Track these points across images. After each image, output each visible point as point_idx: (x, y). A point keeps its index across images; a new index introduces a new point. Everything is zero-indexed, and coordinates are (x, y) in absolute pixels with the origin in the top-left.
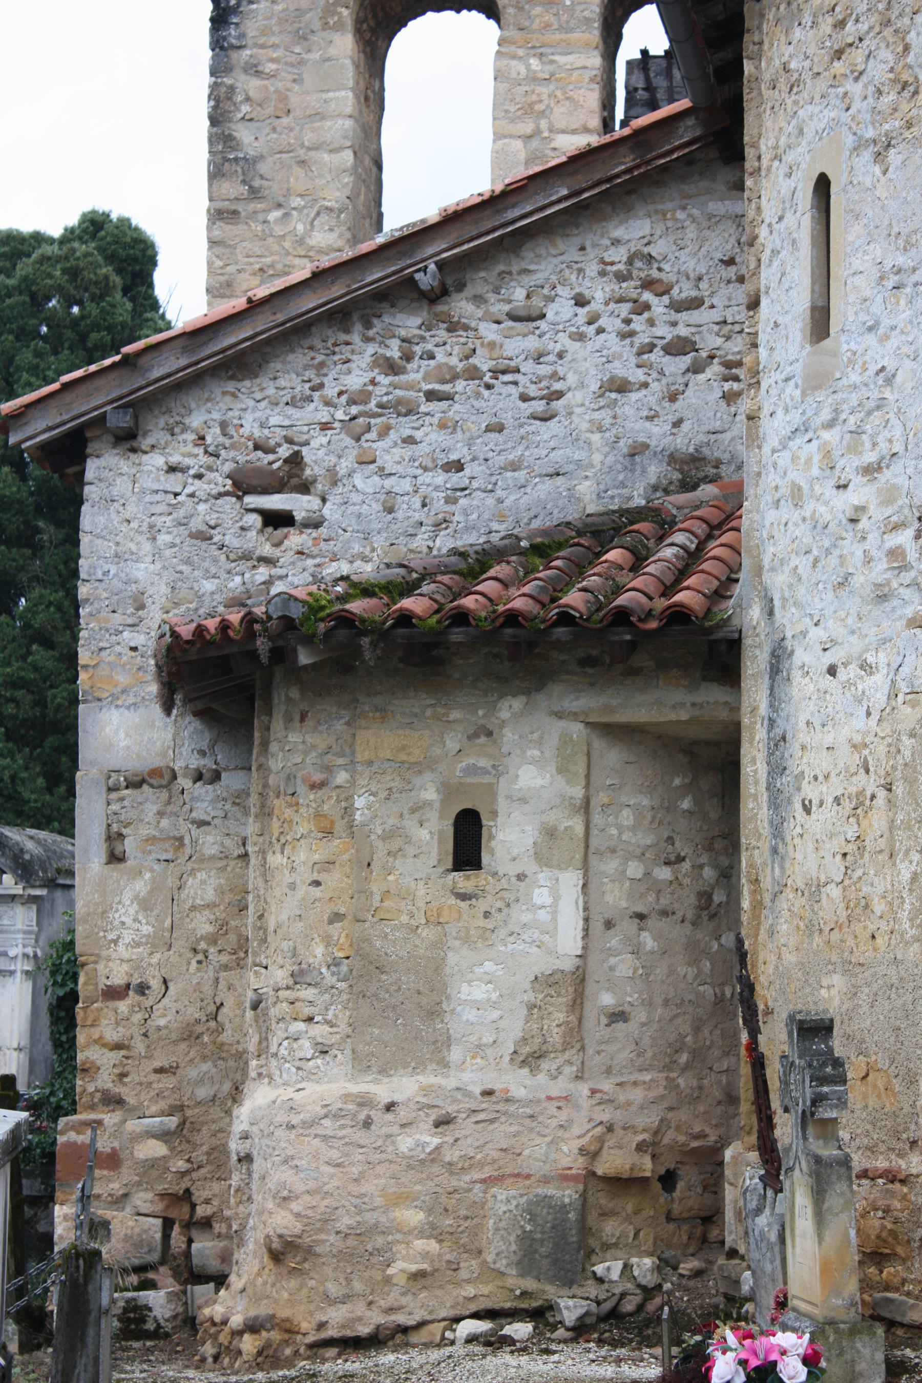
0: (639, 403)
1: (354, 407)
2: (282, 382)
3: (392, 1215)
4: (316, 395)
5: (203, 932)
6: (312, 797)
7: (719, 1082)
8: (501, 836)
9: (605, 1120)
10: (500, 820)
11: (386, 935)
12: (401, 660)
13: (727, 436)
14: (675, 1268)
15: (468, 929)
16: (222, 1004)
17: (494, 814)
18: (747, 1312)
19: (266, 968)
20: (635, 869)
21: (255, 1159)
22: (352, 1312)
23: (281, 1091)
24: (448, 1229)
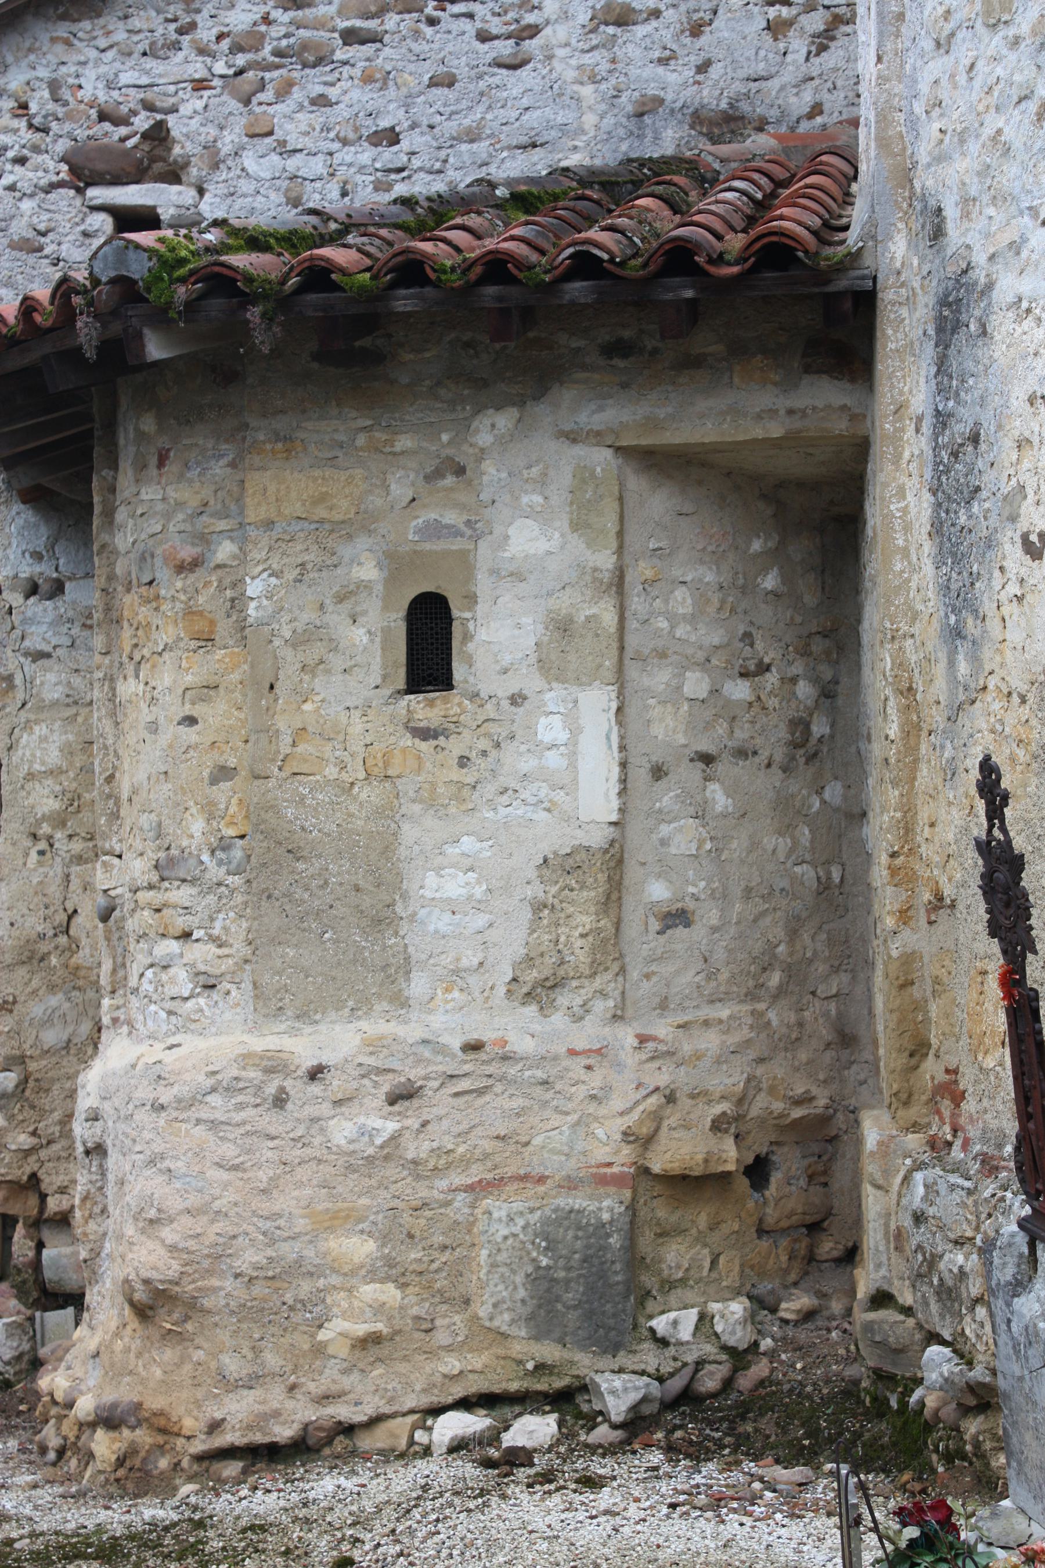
0: (648, 40)
1: (240, 55)
2: (136, 23)
3: (323, 1246)
4: (186, 39)
5: (46, 809)
6: (179, 584)
7: (826, 1014)
8: (482, 635)
9: (662, 1084)
10: (481, 608)
11: (303, 798)
12: (316, 357)
13: (775, 84)
14: (774, 1310)
15: (433, 786)
16: (75, 911)
17: (471, 599)
18: (922, 1404)
19: (120, 857)
20: (696, 684)
21: (110, 1152)
22: (264, 1402)
23: (143, 1048)
24: (414, 1266)
